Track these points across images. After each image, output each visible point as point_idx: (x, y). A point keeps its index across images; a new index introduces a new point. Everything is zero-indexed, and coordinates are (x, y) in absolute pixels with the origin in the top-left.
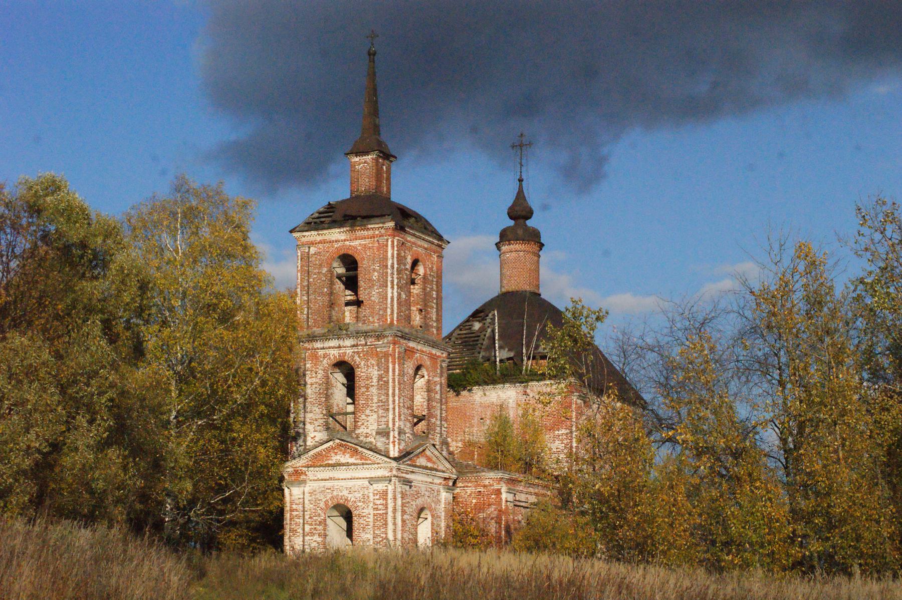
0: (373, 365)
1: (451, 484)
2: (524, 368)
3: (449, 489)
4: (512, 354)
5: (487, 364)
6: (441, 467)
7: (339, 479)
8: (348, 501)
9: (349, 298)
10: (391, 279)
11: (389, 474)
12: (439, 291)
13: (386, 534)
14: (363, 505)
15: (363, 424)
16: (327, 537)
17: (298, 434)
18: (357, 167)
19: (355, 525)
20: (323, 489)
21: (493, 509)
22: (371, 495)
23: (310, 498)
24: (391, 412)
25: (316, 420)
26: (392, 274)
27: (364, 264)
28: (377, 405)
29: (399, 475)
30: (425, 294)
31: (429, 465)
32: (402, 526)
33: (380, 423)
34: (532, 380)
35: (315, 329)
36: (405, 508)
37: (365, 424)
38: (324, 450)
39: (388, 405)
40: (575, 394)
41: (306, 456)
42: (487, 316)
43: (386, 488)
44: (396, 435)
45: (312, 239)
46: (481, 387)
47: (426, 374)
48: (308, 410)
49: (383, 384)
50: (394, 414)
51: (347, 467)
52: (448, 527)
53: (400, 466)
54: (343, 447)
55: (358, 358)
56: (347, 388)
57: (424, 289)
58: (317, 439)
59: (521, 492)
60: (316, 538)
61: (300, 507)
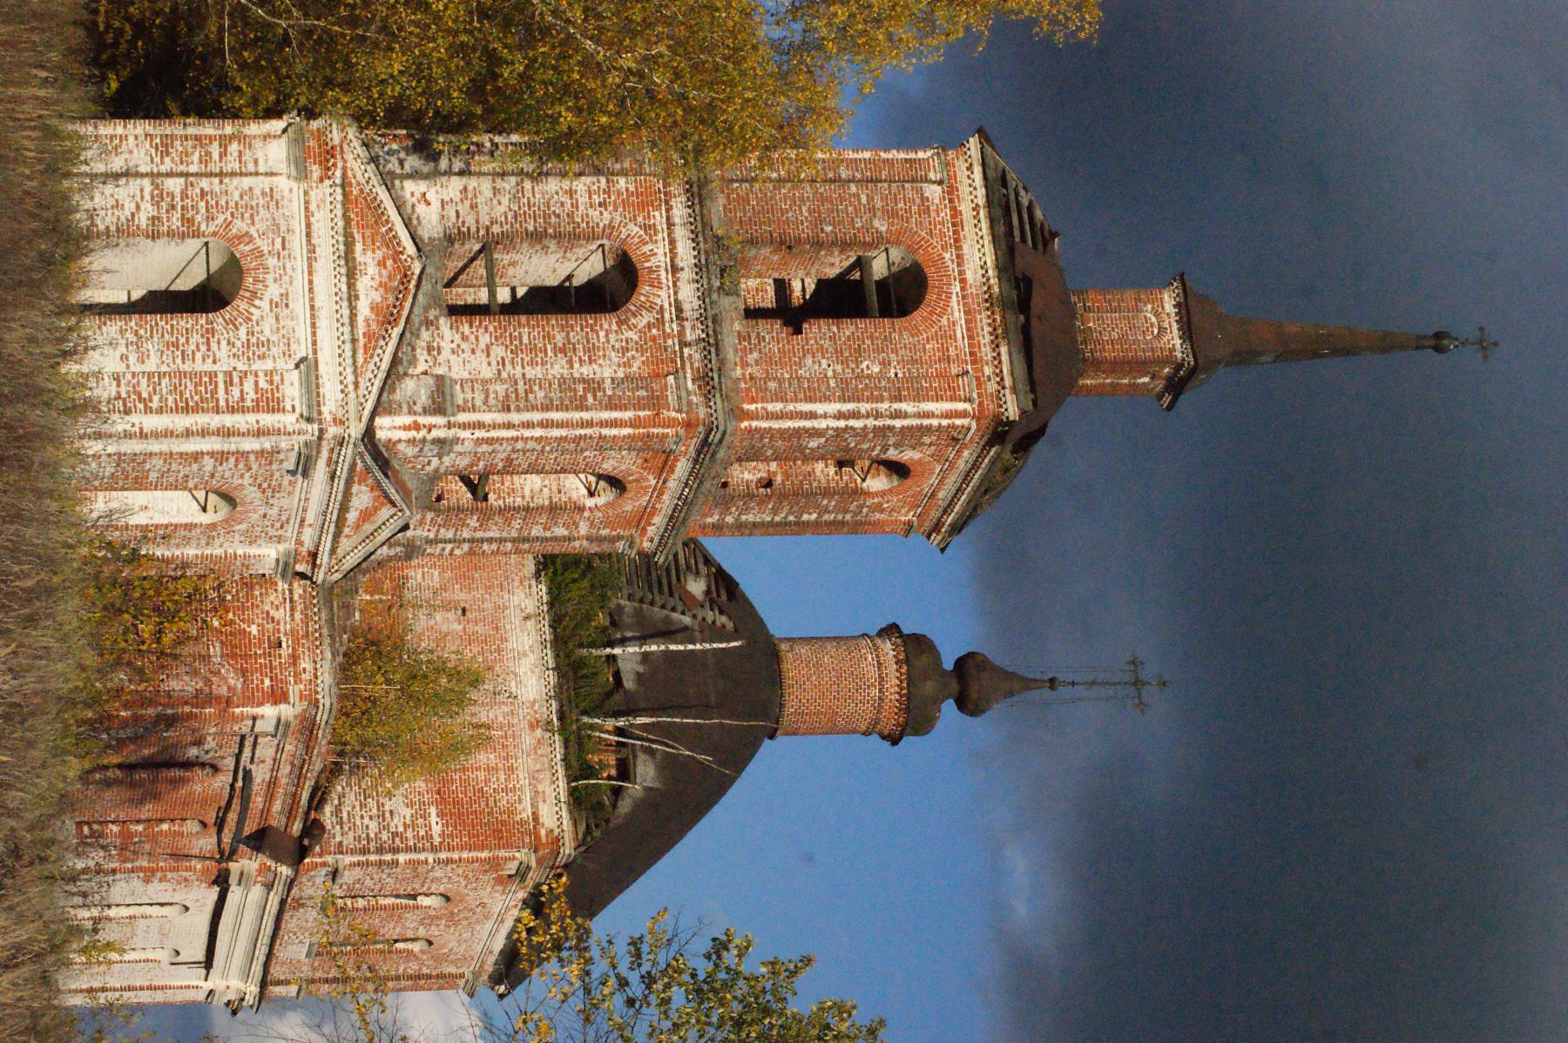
0: (628, 364)
1: (300, 568)
2: (596, 720)
3: (286, 564)
4: (629, 683)
5: (602, 619)
6: (345, 544)
7: (310, 273)
8: (250, 302)
9: (796, 286)
10: (863, 411)
11: (327, 416)
12: (816, 527)
13: (160, 411)
14: (239, 344)
15: (465, 338)
16: (149, 240)
17: (434, 157)
18: (1149, 307)
19: (184, 321)
20: (283, 228)
21: (232, 682)
22: (269, 365)
23: (257, 192)
24: (500, 418)
25: (473, 207)
26: (878, 415)
27: (901, 334)
28: (519, 376)
29: (324, 443)
30: (810, 495)
31: (352, 516)
32: (181, 454)
33: (467, 388)
34: (566, 743)
35: (722, 200)
36: (232, 460)
37: (464, 346)
38: (391, 230)
39: (518, 410)
40: (533, 856)
41: (374, 181)
42: (721, 612)
43: (289, 408)
44: (435, 433)
45: (964, 189)
46: (545, 608)
47: (600, 500)
48: (499, 183)
49: (576, 394)
50: (495, 426)
51: (345, 296)
52: (185, 565)
53: (351, 446)
54: (400, 284)
55: (645, 321)
56: (560, 287)
57: (827, 492)
58: (421, 209)
59: (279, 749)
60: (148, 209)
61: (232, 164)
